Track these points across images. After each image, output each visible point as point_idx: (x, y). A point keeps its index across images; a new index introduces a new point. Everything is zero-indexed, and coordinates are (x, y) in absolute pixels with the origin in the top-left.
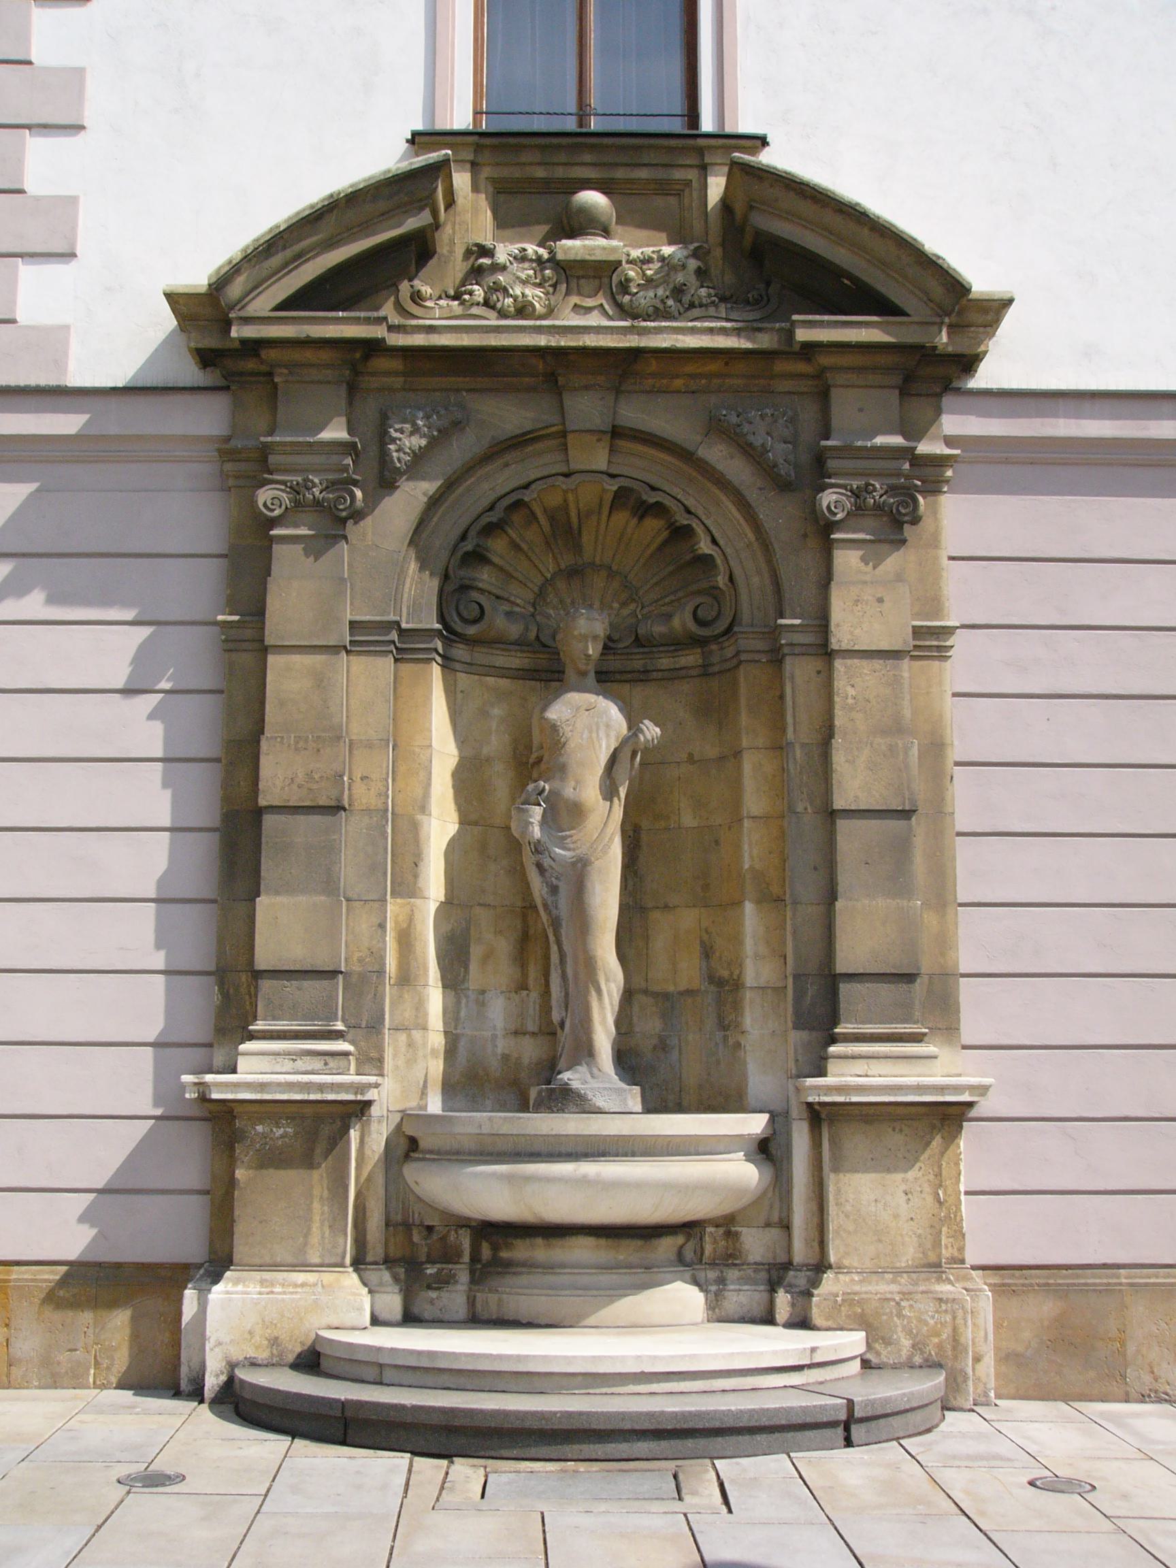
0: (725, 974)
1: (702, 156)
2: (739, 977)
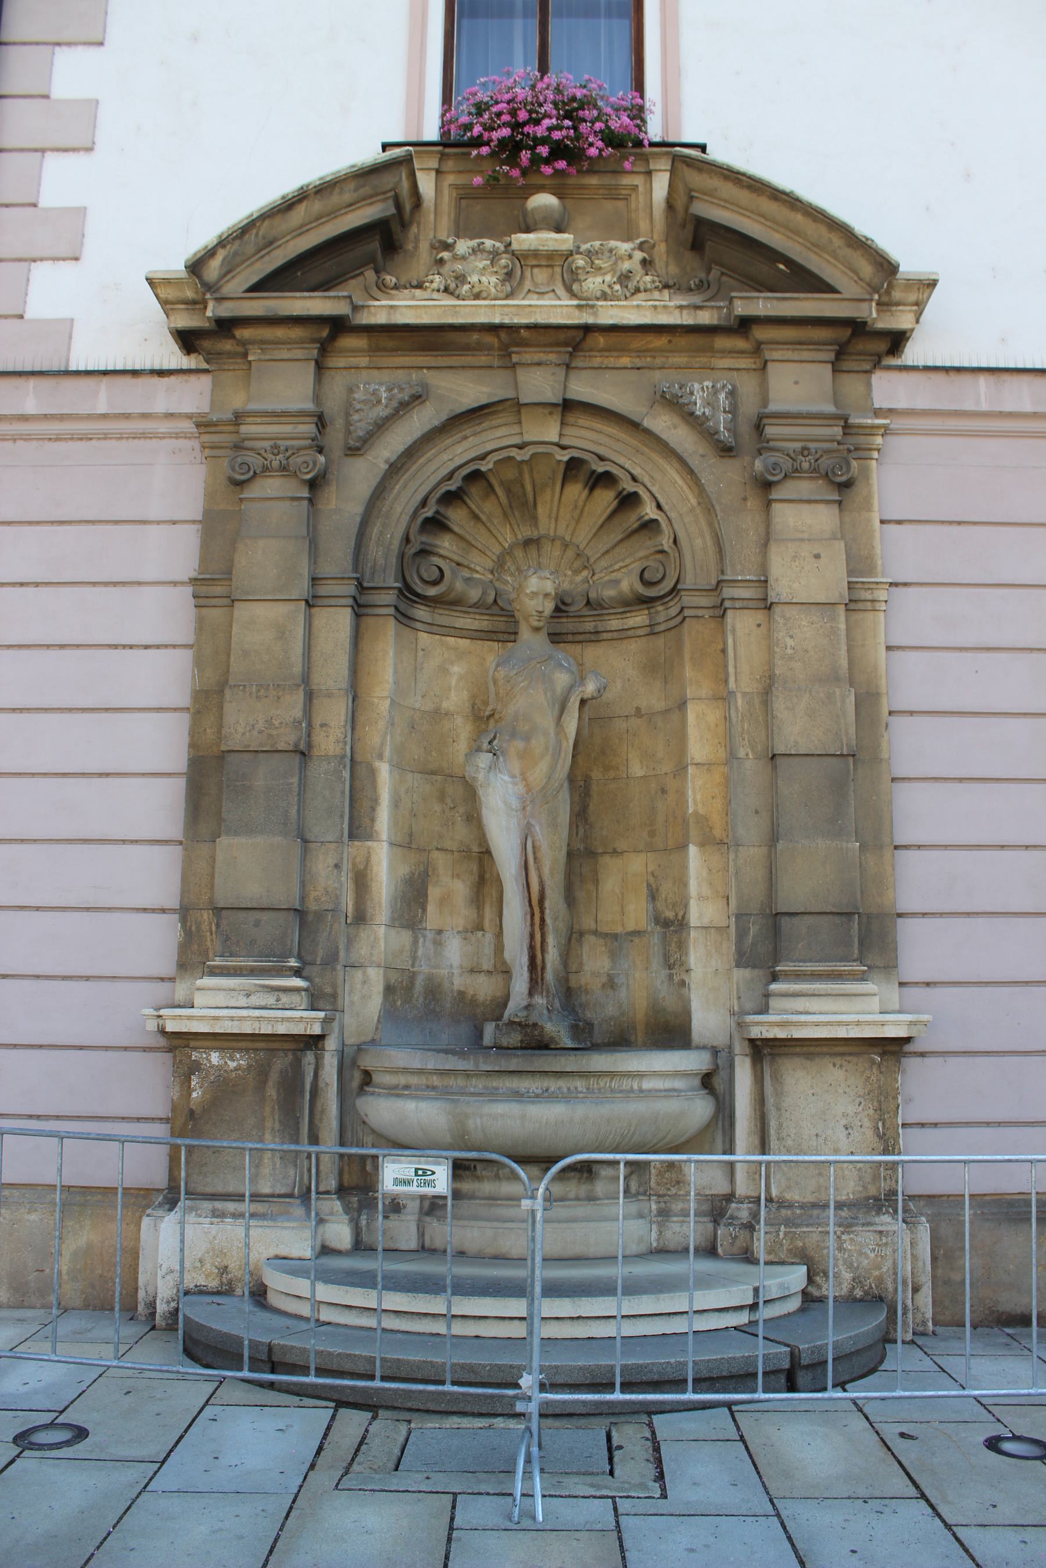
0: (670, 914)
1: (647, 161)
2: (683, 917)
